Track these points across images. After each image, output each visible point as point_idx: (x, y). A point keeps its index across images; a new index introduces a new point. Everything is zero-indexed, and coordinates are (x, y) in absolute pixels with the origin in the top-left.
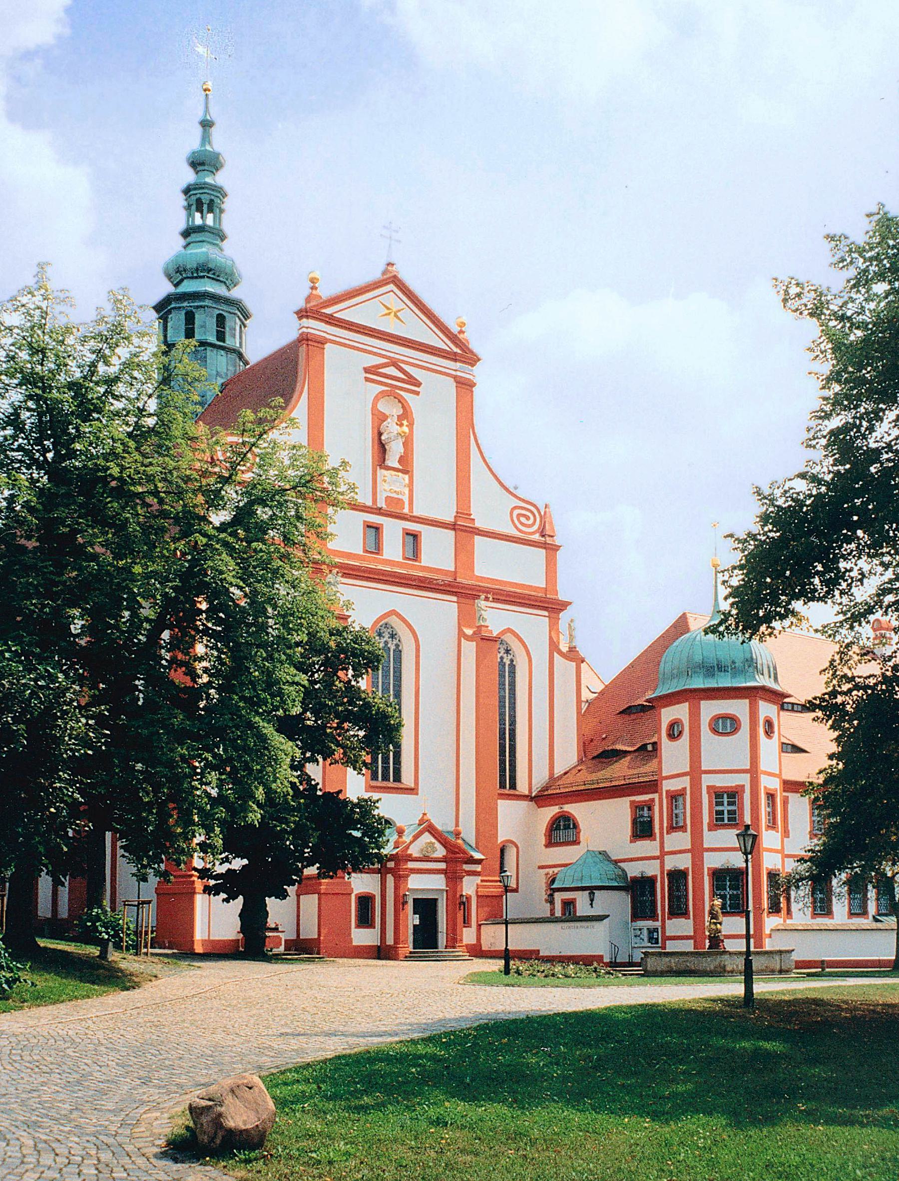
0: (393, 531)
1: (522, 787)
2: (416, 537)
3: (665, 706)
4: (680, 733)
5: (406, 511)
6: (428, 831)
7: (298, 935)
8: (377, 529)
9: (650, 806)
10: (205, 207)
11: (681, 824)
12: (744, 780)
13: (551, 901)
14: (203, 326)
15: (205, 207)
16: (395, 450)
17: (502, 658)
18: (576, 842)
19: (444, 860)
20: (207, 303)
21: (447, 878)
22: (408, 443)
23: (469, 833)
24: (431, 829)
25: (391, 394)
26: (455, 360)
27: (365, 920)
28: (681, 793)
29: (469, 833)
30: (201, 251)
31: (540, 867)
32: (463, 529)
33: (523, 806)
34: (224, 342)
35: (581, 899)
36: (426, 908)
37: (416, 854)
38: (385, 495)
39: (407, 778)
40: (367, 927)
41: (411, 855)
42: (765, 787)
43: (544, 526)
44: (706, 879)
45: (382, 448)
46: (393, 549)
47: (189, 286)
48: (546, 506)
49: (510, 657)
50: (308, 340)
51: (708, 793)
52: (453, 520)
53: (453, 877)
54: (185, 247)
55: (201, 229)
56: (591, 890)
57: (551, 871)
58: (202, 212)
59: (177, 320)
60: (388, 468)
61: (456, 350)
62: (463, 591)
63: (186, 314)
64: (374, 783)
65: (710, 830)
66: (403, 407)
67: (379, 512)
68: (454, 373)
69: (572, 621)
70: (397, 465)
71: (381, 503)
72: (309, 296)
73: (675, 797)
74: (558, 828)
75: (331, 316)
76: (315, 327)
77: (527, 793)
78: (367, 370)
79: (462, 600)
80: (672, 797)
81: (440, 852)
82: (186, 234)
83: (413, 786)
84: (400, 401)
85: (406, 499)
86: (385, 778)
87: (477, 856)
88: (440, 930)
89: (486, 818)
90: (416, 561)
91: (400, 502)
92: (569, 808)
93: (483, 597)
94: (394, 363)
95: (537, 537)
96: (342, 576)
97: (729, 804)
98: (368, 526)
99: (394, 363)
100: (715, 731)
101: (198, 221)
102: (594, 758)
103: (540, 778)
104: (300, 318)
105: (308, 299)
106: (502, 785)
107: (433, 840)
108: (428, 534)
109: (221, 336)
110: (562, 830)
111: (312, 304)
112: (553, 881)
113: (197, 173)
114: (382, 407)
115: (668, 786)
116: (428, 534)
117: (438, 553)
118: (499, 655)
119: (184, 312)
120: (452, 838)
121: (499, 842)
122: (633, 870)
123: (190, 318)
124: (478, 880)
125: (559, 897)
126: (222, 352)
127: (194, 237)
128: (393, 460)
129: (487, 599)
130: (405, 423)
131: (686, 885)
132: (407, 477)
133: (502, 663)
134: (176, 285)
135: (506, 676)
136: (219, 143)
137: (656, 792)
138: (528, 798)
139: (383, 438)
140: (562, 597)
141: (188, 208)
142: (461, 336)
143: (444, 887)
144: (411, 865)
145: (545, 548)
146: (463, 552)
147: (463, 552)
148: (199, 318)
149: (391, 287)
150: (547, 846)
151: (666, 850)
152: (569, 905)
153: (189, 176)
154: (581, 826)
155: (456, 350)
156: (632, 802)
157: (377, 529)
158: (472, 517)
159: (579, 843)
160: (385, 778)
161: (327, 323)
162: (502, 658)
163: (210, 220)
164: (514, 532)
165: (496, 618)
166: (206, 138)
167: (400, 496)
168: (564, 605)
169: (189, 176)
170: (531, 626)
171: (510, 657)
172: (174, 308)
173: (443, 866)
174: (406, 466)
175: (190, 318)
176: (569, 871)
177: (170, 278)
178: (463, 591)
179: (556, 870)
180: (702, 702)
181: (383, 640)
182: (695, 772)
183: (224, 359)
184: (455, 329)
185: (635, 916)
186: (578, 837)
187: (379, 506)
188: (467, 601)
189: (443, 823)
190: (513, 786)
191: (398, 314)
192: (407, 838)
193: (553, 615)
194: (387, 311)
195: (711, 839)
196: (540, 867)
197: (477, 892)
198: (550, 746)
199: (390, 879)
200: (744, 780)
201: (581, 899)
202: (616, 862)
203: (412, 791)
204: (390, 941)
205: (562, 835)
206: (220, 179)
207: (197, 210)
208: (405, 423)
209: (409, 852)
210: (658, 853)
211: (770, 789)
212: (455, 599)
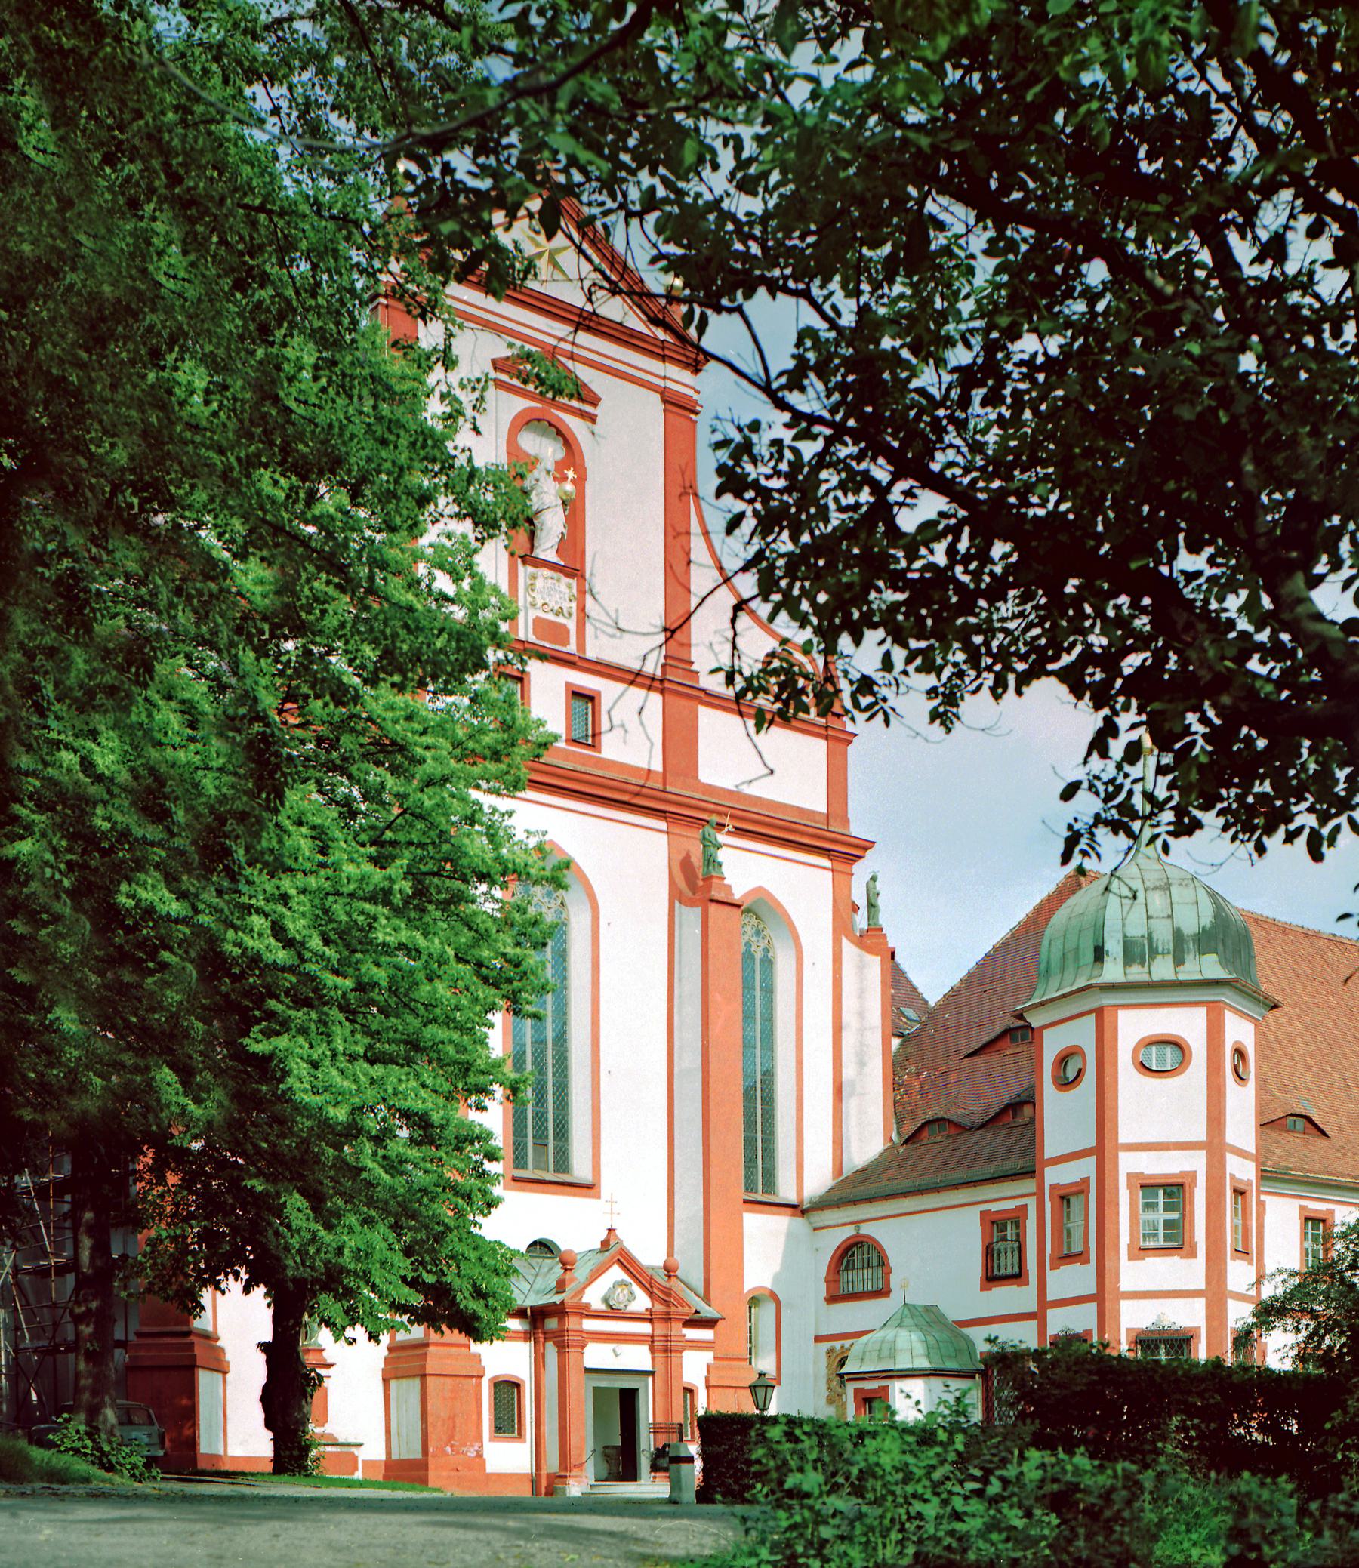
4: (1080, 1073)
5: (572, 648)
7: (389, 1453)
9: (1017, 1218)
11: (1077, 1247)
12: (1196, 1163)
17: (748, 944)
18: (883, 1292)
19: (649, 1317)
21: (652, 1350)
22: (574, 509)
23: (691, 1270)
24: (626, 1261)
26: (664, 358)
28: (1081, 1188)
29: (691, 1270)
31: (818, 1339)
37: (597, 1305)
38: (533, 614)
39: (580, 1169)
41: (587, 1306)
42: (1232, 1177)
51: (1129, 1186)
53: (666, 1349)
57: (837, 1344)
65: (1131, 1258)
66: (567, 443)
68: (661, 383)
69: (874, 879)
70: (551, 556)
80: (1062, 1198)
81: (641, 1302)
84: (559, 433)
85: (571, 625)
87: (708, 1312)
89: (720, 1247)
90: (592, 746)
91: (558, 632)
97: (1168, 1208)
100: (1144, 1068)
103: (818, 1180)
106: (750, 1187)
107: (628, 1279)
112: (842, 1363)
115: (1053, 1176)
117: (633, 735)
120: (661, 1278)
124: (708, 1356)
128: (546, 549)
130: (570, 474)
132: (573, 582)
133: (748, 956)
138: (796, 1209)
140: (858, 829)
144: (589, 1325)
145: (827, 738)
146: (680, 741)
147: (680, 741)
151: (1049, 1298)
154: (893, 1261)
158: (694, 667)
162: (748, 944)
165: (745, 867)
167: (561, 620)
168: (866, 846)
170: (799, 886)
174: (572, 567)
179: (847, 1343)
182: (1103, 1148)
186: (887, 1282)
187: (522, 636)
189: (651, 1254)
190: (770, 1183)
192: (581, 1273)
193: (840, 867)
195: (1132, 1274)
196: (818, 1339)
197: (707, 1380)
198: (836, 1111)
200: (1196, 1163)
203: (588, 1188)
204: (552, 1464)
208: (570, 474)
209: (585, 1300)
210: (1050, 1313)
211: (1241, 1181)
212: (662, 825)
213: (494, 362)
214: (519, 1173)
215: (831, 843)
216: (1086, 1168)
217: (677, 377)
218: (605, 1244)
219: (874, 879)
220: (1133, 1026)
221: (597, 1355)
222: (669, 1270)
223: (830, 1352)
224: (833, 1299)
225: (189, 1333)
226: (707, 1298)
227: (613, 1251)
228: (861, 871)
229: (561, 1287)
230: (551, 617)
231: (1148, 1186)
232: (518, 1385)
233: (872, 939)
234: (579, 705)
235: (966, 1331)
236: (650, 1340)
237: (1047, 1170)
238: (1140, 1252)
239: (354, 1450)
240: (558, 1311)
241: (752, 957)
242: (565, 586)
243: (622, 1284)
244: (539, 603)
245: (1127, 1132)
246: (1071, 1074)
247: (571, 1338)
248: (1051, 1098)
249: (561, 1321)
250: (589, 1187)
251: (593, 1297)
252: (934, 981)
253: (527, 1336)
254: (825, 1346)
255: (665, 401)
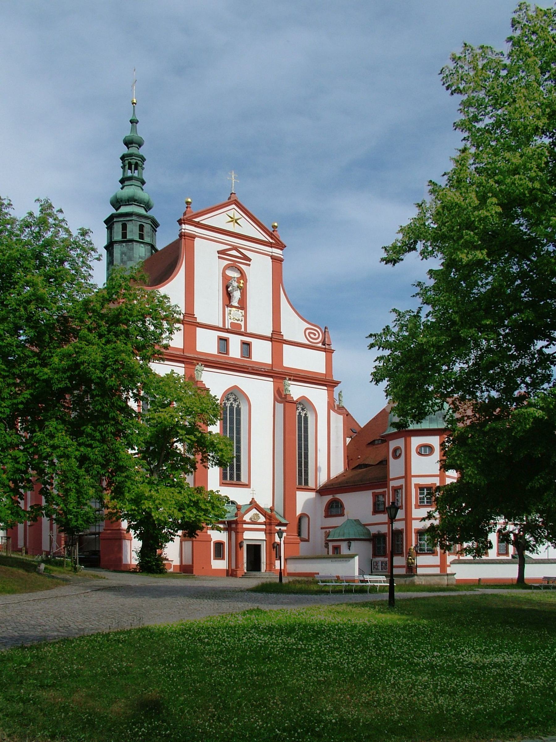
0: (235, 342)
1: (311, 484)
2: (248, 344)
3: (391, 440)
4: (400, 455)
6: (255, 508)
8: (226, 340)
10: (133, 166)
13: (327, 546)
14: (132, 231)
15: (133, 166)
16: (237, 295)
18: (342, 515)
19: (265, 523)
20: (134, 218)
21: (266, 533)
22: (243, 291)
23: (279, 508)
25: (233, 267)
26: (271, 247)
27: (219, 555)
28: (400, 487)
30: (130, 191)
31: (322, 528)
32: (277, 339)
33: (312, 495)
34: (143, 239)
35: (344, 546)
36: (254, 550)
37: (248, 520)
38: (230, 321)
39: (244, 480)
40: (221, 559)
41: (245, 521)
43: (325, 339)
44: (413, 535)
45: (228, 295)
46: (235, 352)
47: (124, 209)
48: (325, 328)
49: (304, 412)
50: (184, 236)
52: (270, 336)
53: (269, 533)
54: (122, 188)
55: (130, 179)
56: (349, 541)
57: (328, 530)
58: (131, 170)
59: (118, 228)
60: (232, 306)
61: (271, 241)
62: (277, 374)
63: (122, 225)
64: (224, 482)
66: (241, 273)
67: (228, 331)
68: (271, 254)
69: (341, 392)
71: (228, 326)
72: (186, 212)
73: (396, 490)
74: (332, 507)
75: (198, 223)
76: (188, 228)
77: (314, 488)
78: (219, 252)
79: (275, 380)
81: (262, 519)
82: (122, 181)
83: (247, 483)
84: (238, 270)
85: (242, 324)
86: (231, 478)
87: (284, 521)
88: (262, 561)
89: (289, 500)
92: (338, 496)
93: (288, 379)
94: (235, 248)
95: (320, 345)
96: (204, 367)
98: (221, 339)
99: (235, 248)
100: (420, 454)
101: (129, 173)
102: (353, 469)
103: (323, 479)
104: (180, 224)
105: (185, 214)
106: (300, 483)
107: (258, 513)
108: (256, 344)
109: (141, 236)
110: (334, 509)
111: (187, 216)
113: (128, 149)
114: (230, 273)
115: (392, 484)
116: (256, 344)
117: (262, 353)
118: (298, 411)
119: (121, 223)
120: (269, 512)
121: (297, 514)
122: (374, 530)
123: (124, 227)
125: (331, 545)
126: (142, 245)
127: (126, 183)
128: (235, 303)
129: (290, 379)
130: (242, 281)
131: (402, 539)
132: (243, 311)
134: (117, 210)
135: (303, 422)
136: (142, 132)
137: (386, 487)
139: (229, 289)
140: (335, 379)
141: (123, 167)
142: (274, 233)
143: (265, 538)
144: (245, 526)
145: (325, 352)
146: (277, 355)
147: (277, 355)
148: (129, 226)
149: (234, 206)
150: (326, 517)
152: (337, 549)
153: (125, 150)
155: (271, 241)
156: (373, 493)
157: (226, 340)
159: (344, 515)
160: (231, 478)
161: (195, 226)
162: (300, 413)
163: (136, 174)
164: (307, 342)
165: (296, 391)
166: (134, 129)
167: (239, 322)
168: (338, 383)
169: (125, 150)
170: (318, 396)
171: (304, 412)
172: (116, 222)
173: (264, 527)
174: (242, 305)
175: (124, 227)
176: (338, 531)
177: (113, 205)
178: (277, 374)
179: (331, 530)
180: (412, 438)
181: (229, 402)
182: (407, 476)
183: (143, 249)
184: (271, 230)
185: (375, 555)
187: (227, 327)
188: (279, 381)
191: (238, 221)
192: (243, 511)
193: (330, 389)
194: (230, 219)
196: (322, 528)
198: (329, 458)
199: (233, 534)
201: (344, 546)
202: (365, 525)
203: (247, 486)
204: (233, 567)
205: (334, 511)
206: (142, 151)
207: (129, 169)
208: (242, 281)
209: (244, 519)
212: (272, 379)
213: (218, 252)
214: (224, 482)
215: (327, 382)
216: (402, 482)
217: (277, 252)
218: (251, 503)
219: (341, 392)
220: (416, 441)
221: (247, 535)
222: (272, 509)
223: (326, 532)
224: (326, 516)
225: (120, 530)
226: (284, 517)
227: (253, 504)
228: (337, 390)
229: (236, 515)
230: (236, 322)
231: (421, 488)
232: (223, 544)
233: (341, 410)
234: (245, 346)
235: (367, 527)
236: (265, 530)
237: (391, 482)
238: (418, 507)
239: (171, 562)
240: (236, 522)
241: (301, 416)
242: (240, 313)
243: (256, 514)
244: (232, 318)
245: (414, 471)
246: (398, 455)
247: (239, 530)
248: (392, 462)
249: (236, 526)
250: (247, 485)
251: (247, 518)
252: (363, 421)
253: (225, 529)
254: (324, 530)
255: (272, 259)
